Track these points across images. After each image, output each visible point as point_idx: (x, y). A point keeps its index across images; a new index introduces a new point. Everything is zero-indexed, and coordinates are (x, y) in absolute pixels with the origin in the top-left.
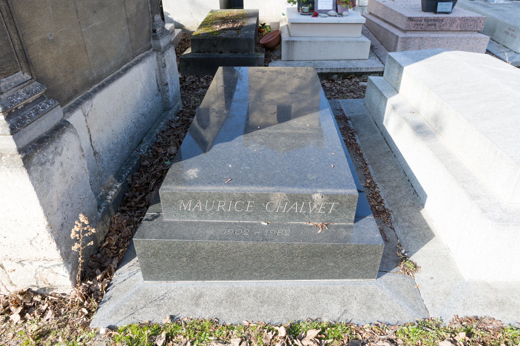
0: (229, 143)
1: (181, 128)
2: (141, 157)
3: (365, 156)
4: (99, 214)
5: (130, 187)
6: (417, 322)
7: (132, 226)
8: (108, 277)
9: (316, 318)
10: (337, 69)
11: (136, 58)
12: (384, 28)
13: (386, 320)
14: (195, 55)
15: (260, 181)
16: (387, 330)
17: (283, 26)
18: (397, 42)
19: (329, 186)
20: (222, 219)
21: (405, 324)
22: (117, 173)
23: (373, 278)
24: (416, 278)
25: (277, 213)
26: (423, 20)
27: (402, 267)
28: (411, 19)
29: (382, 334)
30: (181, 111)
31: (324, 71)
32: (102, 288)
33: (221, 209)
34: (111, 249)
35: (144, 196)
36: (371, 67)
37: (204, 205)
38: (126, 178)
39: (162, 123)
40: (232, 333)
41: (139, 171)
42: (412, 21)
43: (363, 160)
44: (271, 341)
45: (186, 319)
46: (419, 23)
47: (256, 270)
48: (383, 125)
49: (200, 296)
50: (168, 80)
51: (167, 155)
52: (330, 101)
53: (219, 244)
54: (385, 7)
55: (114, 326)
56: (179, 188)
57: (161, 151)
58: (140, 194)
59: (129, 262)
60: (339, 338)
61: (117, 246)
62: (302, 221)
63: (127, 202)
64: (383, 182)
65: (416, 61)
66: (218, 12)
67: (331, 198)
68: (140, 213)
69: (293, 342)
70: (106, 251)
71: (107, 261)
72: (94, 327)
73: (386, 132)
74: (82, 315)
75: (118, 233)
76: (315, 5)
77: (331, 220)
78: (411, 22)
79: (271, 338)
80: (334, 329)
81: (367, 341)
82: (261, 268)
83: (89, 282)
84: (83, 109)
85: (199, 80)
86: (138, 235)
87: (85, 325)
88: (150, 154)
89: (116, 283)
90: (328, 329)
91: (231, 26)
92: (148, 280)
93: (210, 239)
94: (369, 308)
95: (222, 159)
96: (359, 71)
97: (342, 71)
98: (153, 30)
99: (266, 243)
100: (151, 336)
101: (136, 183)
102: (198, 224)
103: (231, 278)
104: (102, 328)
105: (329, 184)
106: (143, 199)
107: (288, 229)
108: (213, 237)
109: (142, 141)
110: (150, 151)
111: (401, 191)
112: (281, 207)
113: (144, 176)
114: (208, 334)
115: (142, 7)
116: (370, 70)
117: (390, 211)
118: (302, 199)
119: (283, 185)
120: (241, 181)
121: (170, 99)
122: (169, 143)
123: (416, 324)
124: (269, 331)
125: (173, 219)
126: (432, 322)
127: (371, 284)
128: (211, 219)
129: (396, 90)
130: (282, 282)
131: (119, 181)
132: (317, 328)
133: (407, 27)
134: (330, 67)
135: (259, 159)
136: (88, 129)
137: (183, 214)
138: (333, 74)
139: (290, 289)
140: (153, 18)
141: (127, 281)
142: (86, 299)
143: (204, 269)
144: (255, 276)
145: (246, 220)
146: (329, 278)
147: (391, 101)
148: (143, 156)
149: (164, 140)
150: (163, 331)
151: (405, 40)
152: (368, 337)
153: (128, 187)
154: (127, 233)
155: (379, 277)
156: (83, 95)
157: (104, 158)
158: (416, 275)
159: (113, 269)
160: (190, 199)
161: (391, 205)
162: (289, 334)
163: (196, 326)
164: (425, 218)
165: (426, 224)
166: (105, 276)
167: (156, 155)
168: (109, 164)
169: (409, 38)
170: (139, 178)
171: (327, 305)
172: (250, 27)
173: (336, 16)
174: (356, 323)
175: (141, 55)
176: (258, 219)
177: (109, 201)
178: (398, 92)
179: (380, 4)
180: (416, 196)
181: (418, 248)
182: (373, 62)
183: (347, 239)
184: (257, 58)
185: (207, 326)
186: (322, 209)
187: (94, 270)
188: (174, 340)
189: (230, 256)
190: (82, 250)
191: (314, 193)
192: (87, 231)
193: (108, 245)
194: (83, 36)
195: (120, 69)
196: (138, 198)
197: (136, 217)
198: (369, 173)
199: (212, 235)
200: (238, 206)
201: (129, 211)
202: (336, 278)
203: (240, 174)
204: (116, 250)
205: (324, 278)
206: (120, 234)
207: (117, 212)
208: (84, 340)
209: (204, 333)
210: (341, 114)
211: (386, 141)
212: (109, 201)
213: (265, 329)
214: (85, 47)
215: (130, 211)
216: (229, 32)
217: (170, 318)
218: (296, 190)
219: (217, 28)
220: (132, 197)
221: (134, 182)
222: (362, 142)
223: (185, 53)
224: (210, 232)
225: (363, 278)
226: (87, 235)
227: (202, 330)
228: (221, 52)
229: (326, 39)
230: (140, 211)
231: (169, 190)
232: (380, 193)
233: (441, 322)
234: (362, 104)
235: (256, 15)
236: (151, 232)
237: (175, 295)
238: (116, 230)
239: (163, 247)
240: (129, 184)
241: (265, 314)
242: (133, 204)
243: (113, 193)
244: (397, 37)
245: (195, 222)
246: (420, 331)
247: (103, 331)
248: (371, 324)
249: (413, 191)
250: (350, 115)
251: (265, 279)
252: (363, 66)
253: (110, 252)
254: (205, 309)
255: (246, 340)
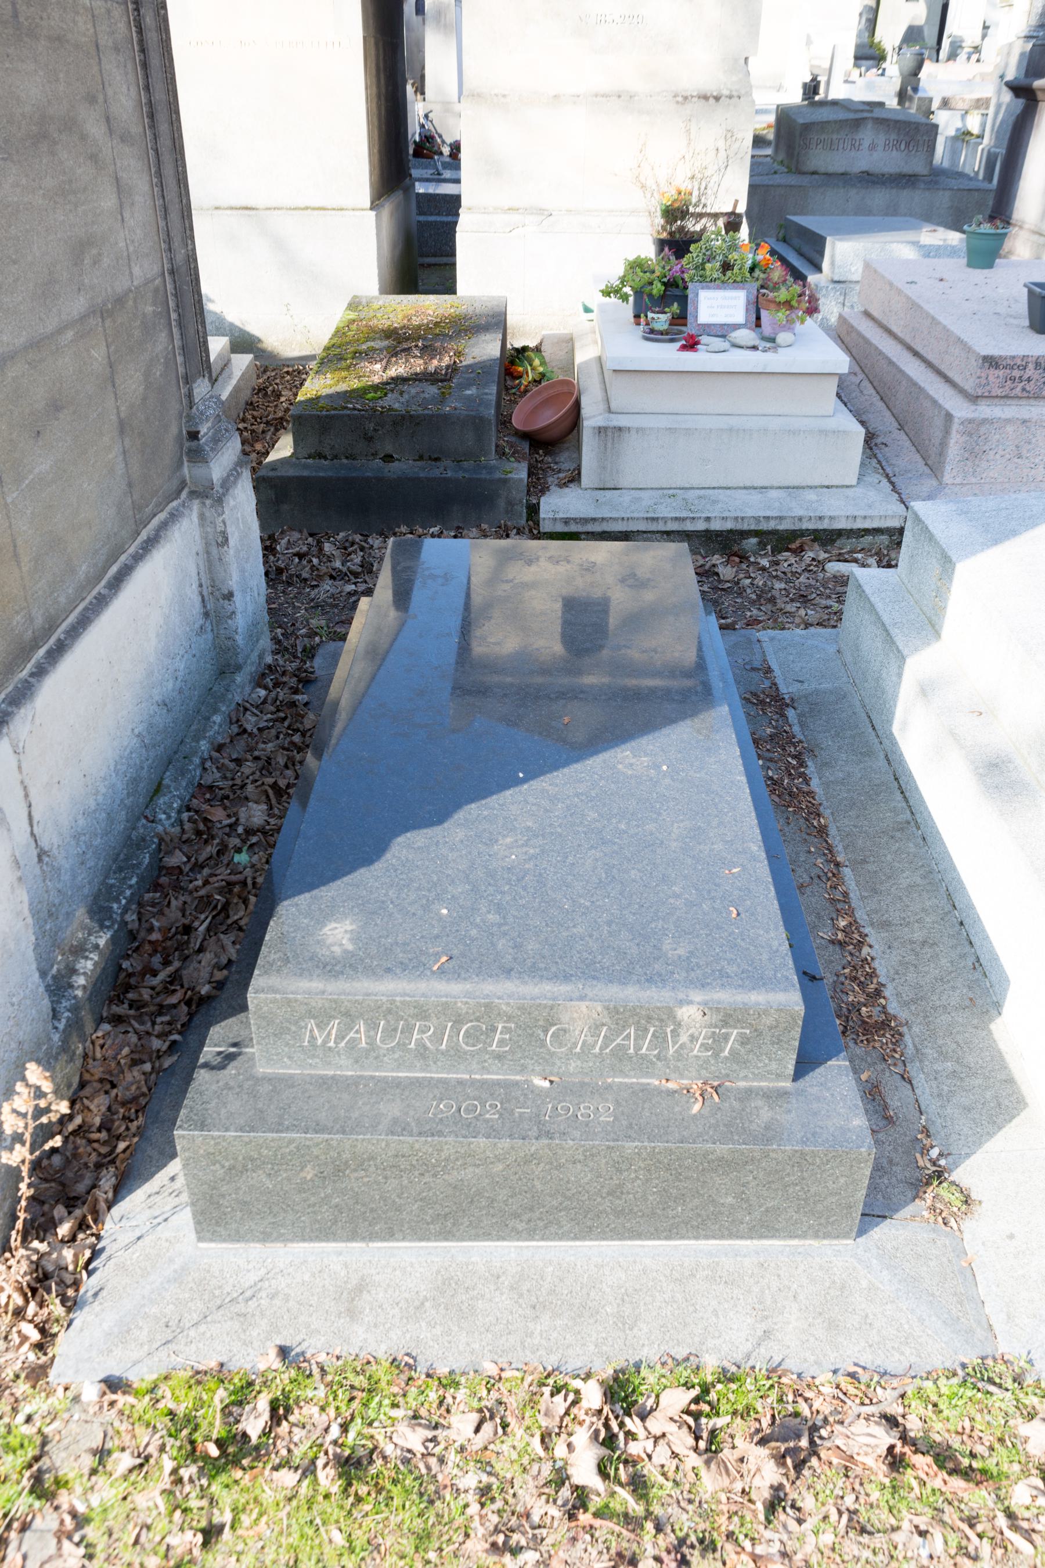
0: (436, 831)
1: (273, 732)
2: (161, 840)
3: (834, 837)
4: (56, 1037)
5: (135, 939)
6: (964, 1366)
7: (147, 1067)
8: (89, 1227)
9: (685, 1354)
10: (757, 519)
11: (144, 535)
12: (909, 379)
13: (878, 1362)
14: (306, 467)
15: (529, 963)
16: (878, 1389)
17: (586, 363)
18: (947, 432)
19: (723, 979)
20: (422, 1070)
21: (929, 1373)
22: (96, 897)
23: (846, 1236)
24: (967, 1236)
25: (578, 1056)
26: (1031, 366)
27: (929, 1202)
28: (991, 362)
29: (867, 1401)
30: (269, 667)
31: (716, 526)
32: (76, 1263)
33: (420, 1043)
34: (90, 1142)
35: (177, 971)
36: (862, 513)
37: (372, 1033)
38: (123, 914)
39: (217, 718)
40: (454, 1398)
41: (156, 887)
42: (997, 367)
43: (830, 848)
44: (562, 1421)
45: (322, 1358)
46: (1016, 373)
47: (516, 1216)
48: (892, 734)
49: (360, 1289)
50: (234, 582)
51: (240, 830)
52: (733, 637)
53: (417, 1146)
54: (914, 306)
55: (120, 1379)
56: (304, 984)
57: (218, 815)
58: (166, 963)
59: (147, 1180)
60: (748, 1414)
61: (109, 1130)
62: (647, 1075)
63: (128, 988)
64: (885, 925)
65: (996, 542)
66: (376, 306)
67: (728, 1018)
68: (169, 1023)
69: (622, 1425)
70: (76, 1148)
71: (82, 1177)
72: (64, 1381)
73: (901, 761)
74: (21, 1344)
75: (108, 1086)
76: (690, 308)
77: (728, 1075)
78: (992, 371)
79: (562, 1412)
80: (733, 1386)
81: (825, 1420)
82: (532, 1209)
83: (36, 1244)
84: (13, 735)
85: (321, 549)
86: (189, 1119)
87: (37, 1374)
88: (187, 826)
89: (115, 1246)
90: (719, 1387)
91: (418, 365)
92: (211, 1240)
93: (393, 1133)
94: (832, 1325)
95: (419, 889)
96: (825, 525)
97: (771, 525)
98: (189, 433)
99: (549, 1145)
100: (226, 1406)
101: (151, 930)
102: (356, 1084)
103: (446, 1235)
104: (87, 1383)
105: (723, 974)
106: (175, 978)
107: (607, 1100)
108: (398, 1127)
109: (160, 785)
110: (185, 816)
111: (936, 957)
112: (590, 1040)
113: (174, 903)
114: (386, 1402)
115: (158, 371)
116: (860, 525)
117: (901, 1025)
118: (649, 1018)
119: (594, 978)
120: (476, 965)
121: (240, 639)
122: (243, 786)
123: (960, 1372)
124: (556, 1391)
125: (283, 1067)
126: (1003, 1368)
127: (840, 1256)
128: (393, 1070)
129: (931, 626)
130: (590, 1247)
131: (102, 927)
132: (688, 1386)
133: (980, 385)
134: (733, 514)
135: (525, 888)
136: (25, 788)
137: (313, 1056)
138: (744, 534)
139: (612, 1269)
140: (190, 395)
141: (146, 1240)
142: (33, 1296)
143: (372, 1210)
144: (514, 1229)
145: (489, 1073)
146: (722, 1237)
147: (919, 665)
148: (167, 839)
149: (225, 778)
150: (259, 1392)
151: (973, 427)
152: (826, 1409)
153: (129, 940)
154: (134, 1088)
155: (862, 1232)
156: (10, 689)
157: (63, 862)
158: (967, 1225)
159: (103, 1205)
160: (335, 1018)
161: (906, 1004)
162: (613, 1403)
163: (351, 1376)
164: (1002, 1046)
165: (1004, 1067)
166: (82, 1225)
167: (204, 831)
168: (74, 877)
169: (984, 421)
170: (161, 913)
171: (717, 1316)
172: (480, 371)
173: (755, 348)
174: (795, 1370)
175: (155, 522)
176: (523, 1069)
177: (79, 993)
178: (937, 635)
179: (899, 292)
180: (979, 982)
181: (979, 1144)
182: (872, 495)
183: (770, 1134)
184: (505, 481)
185: (384, 1379)
186: (702, 1045)
187: (46, 1207)
188: (291, 1418)
189: (446, 1177)
190: (32, 1162)
191: (681, 1003)
192: (47, 1110)
193: (80, 1127)
194: (9, 517)
195: (103, 583)
196: (162, 976)
197: (158, 1036)
198: (846, 894)
199: (395, 1121)
200: (468, 1034)
201: (135, 1017)
202: (742, 1238)
203: (473, 940)
204: (105, 1143)
205: (707, 1237)
206: (115, 1091)
207: (100, 1020)
208: (36, 1417)
209: (377, 1399)
210: (767, 684)
211: (900, 788)
212: (79, 993)
213: (544, 1385)
214: (15, 546)
215: (139, 1018)
216: (413, 391)
217: (278, 1355)
218: (631, 994)
219: (373, 372)
220: (143, 974)
221: (145, 925)
222: (826, 785)
223: (273, 457)
224: (391, 1109)
225: (816, 1236)
226: (44, 1120)
227: (370, 1391)
228: (388, 458)
229: (722, 423)
230: (166, 1018)
231: (275, 991)
232: (876, 964)
233: (1027, 1366)
234: (832, 649)
235: (496, 321)
236: (223, 1111)
237: (288, 1286)
238: (101, 1081)
239: (259, 1153)
240: (131, 931)
241: (544, 1342)
242: (146, 994)
243: (89, 965)
244: (949, 417)
245: (347, 1078)
246: (969, 1393)
247: (91, 1392)
248: (835, 1372)
249: (973, 959)
250: (794, 688)
251: (543, 1239)
252: (839, 511)
253: (89, 1149)
254: (375, 1325)
255: (492, 1418)
